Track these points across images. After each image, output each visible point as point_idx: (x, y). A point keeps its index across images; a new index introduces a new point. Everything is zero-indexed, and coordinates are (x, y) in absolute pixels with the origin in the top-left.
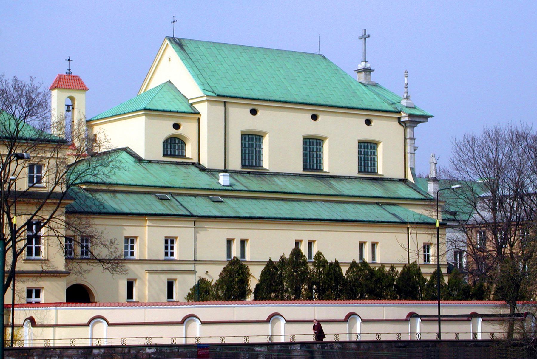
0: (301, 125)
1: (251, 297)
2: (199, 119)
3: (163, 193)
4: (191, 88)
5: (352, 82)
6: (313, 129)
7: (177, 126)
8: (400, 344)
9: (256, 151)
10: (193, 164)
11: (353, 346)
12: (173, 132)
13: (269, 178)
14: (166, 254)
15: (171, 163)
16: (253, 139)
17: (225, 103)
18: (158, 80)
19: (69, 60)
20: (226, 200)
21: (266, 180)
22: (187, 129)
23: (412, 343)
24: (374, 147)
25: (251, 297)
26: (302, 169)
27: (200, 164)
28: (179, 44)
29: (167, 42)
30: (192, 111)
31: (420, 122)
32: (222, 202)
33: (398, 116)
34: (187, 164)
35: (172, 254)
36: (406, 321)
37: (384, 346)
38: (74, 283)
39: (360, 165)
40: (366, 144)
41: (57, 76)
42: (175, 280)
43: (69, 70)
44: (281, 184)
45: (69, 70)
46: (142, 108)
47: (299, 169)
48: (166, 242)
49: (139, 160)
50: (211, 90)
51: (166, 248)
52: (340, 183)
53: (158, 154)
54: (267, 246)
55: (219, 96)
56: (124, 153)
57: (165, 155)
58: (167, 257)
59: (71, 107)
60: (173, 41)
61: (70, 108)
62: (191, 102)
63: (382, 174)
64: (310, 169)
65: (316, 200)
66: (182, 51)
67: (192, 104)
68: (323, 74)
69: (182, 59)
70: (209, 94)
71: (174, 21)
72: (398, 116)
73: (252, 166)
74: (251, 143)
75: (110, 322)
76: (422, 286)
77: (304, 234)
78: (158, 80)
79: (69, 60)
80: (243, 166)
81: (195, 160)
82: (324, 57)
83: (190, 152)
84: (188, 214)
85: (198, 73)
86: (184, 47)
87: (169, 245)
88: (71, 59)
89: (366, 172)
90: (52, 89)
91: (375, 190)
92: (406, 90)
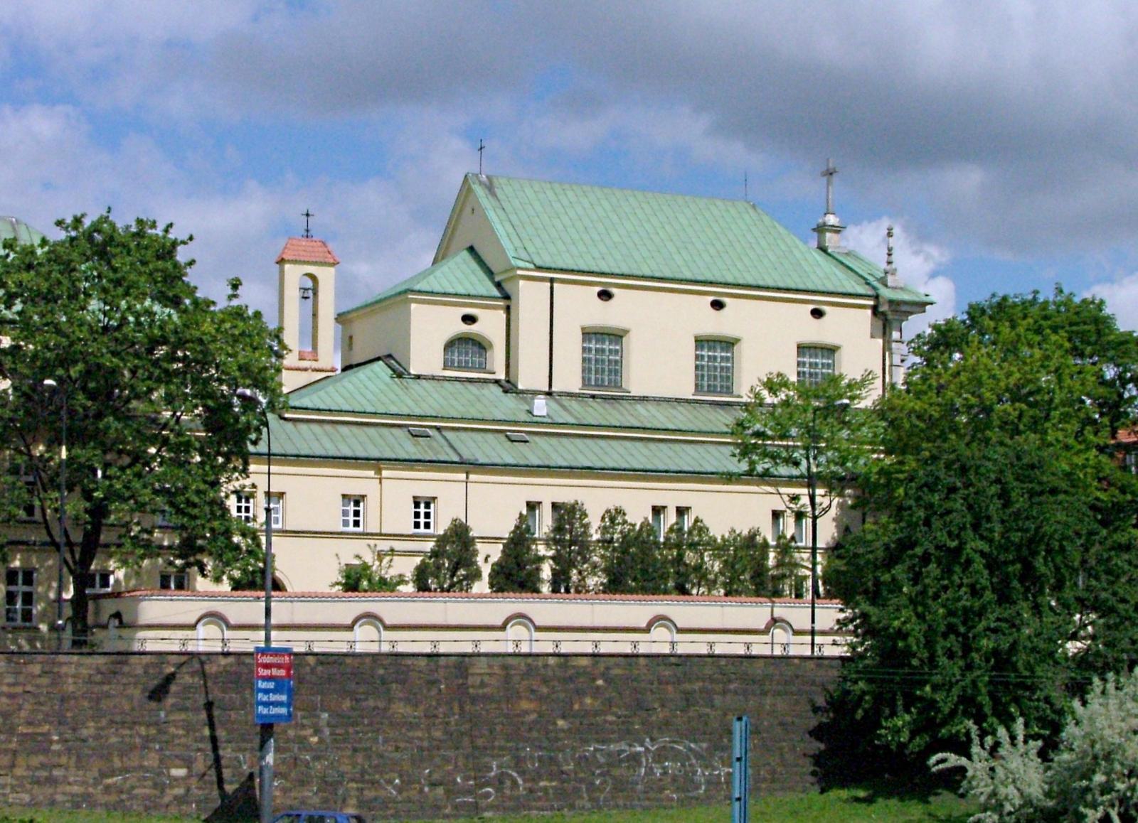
0: (694, 316)
1: (481, 586)
3: (519, 431)
5: (693, 243)
6: (716, 324)
8: (673, 660)
11: (584, 662)
13: (628, 406)
14: (417, 525)
15: (457, 379)
19: (308, 215)
20: (537, 439)
21: (621, 408)
23: (696, 660)
25: (481, 586)
31: (911, 313)
32: (526, 442)
35: (427, 525)
36: (765, 631)
37: (642, 661)
43: (307, 231)
44: (659, 416)
45: (307, 231)
47: (688, 391)
48: (417, 505)
50: (528, 259)
51: (417, 515)
54: (491, 509)
55: (539, 268)
57: (445, 368)
58: (417, 531)
59: (310, 292)
64: (597, 385)
65: (703, 442)
66: (490, 197)
73: (602, 386)
76: (654, 566)
77: (671, 495)
79: (308, 215)
80: (586, 383)
84: (456, 459)
89: (712, 390)
91: (614, 415)
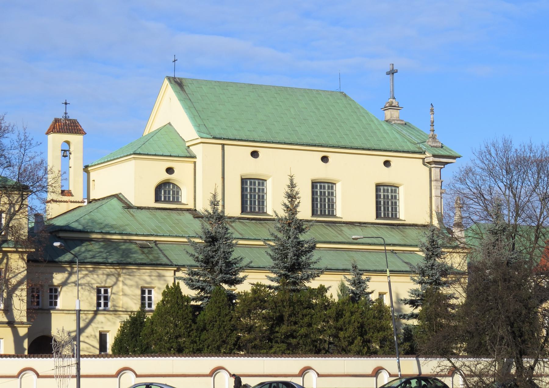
2: (195, 163)
4: (187, 130)
5: (373, 121)
7: (170, 171)
9: (392, 203)
10: (188, 210)
12: (166, 176)
16: (255, 183)
17: (223, 145)
18: (155, 123)
19: (66, 104)
22: (183, 175)
24: (395, 190)
26: (375, 217)
27: (195, 210)
28: (179, 84)
29: (166, 82)
30: (188, 155)
33: (423, 156)
34: (181, 210)
38: (41, 334)
39: (378, 209)
40: (386, 188)
41: (53, 119)
42: (108, 331)
43: (66, 113)
45: (66, 113)
46: (132, 153)
49: (128, 206)
52: (353, 230)
53: (149, 201)
56: (115, 199)
60: (173, 82)
61: (66, 153)
62: (188, 144)
63: (403, 219)
66: (181, 92)
67: (189, 147)
68: (340, 113)
69: (180, 100)
70: (205, 135)
71: (175, 61)
72: (423, 156)
74: (323, 190)
75: (320, 372)
78: (155, 123)
79: (66, 104)
81: (191, 206)
82: (345, 95)
83: (186, 199)
85: (196, 114)
86: (185, 87)
87: (147, 295)
88: (64, 102)
89: (323, 215)
90: (48, 133)
92: (432, 128)
